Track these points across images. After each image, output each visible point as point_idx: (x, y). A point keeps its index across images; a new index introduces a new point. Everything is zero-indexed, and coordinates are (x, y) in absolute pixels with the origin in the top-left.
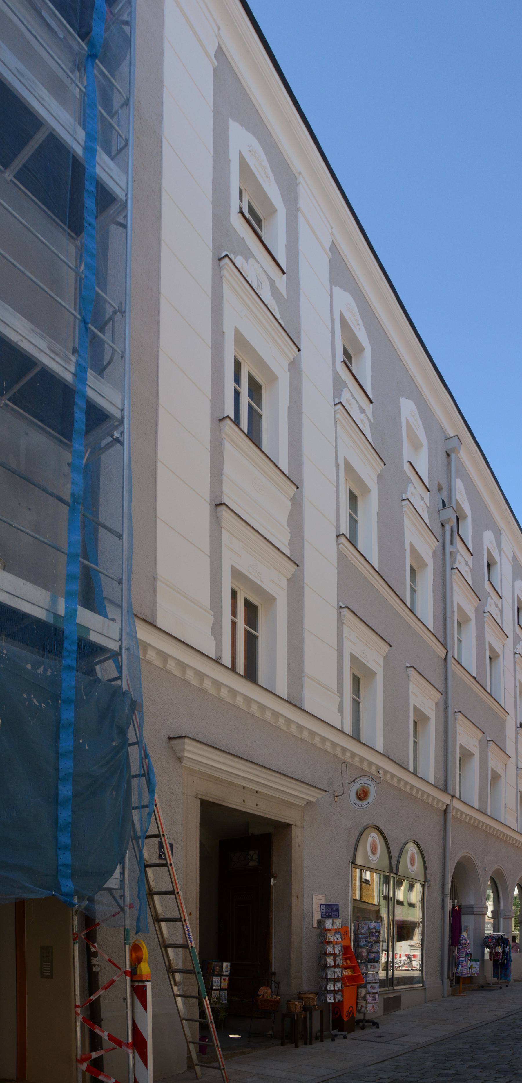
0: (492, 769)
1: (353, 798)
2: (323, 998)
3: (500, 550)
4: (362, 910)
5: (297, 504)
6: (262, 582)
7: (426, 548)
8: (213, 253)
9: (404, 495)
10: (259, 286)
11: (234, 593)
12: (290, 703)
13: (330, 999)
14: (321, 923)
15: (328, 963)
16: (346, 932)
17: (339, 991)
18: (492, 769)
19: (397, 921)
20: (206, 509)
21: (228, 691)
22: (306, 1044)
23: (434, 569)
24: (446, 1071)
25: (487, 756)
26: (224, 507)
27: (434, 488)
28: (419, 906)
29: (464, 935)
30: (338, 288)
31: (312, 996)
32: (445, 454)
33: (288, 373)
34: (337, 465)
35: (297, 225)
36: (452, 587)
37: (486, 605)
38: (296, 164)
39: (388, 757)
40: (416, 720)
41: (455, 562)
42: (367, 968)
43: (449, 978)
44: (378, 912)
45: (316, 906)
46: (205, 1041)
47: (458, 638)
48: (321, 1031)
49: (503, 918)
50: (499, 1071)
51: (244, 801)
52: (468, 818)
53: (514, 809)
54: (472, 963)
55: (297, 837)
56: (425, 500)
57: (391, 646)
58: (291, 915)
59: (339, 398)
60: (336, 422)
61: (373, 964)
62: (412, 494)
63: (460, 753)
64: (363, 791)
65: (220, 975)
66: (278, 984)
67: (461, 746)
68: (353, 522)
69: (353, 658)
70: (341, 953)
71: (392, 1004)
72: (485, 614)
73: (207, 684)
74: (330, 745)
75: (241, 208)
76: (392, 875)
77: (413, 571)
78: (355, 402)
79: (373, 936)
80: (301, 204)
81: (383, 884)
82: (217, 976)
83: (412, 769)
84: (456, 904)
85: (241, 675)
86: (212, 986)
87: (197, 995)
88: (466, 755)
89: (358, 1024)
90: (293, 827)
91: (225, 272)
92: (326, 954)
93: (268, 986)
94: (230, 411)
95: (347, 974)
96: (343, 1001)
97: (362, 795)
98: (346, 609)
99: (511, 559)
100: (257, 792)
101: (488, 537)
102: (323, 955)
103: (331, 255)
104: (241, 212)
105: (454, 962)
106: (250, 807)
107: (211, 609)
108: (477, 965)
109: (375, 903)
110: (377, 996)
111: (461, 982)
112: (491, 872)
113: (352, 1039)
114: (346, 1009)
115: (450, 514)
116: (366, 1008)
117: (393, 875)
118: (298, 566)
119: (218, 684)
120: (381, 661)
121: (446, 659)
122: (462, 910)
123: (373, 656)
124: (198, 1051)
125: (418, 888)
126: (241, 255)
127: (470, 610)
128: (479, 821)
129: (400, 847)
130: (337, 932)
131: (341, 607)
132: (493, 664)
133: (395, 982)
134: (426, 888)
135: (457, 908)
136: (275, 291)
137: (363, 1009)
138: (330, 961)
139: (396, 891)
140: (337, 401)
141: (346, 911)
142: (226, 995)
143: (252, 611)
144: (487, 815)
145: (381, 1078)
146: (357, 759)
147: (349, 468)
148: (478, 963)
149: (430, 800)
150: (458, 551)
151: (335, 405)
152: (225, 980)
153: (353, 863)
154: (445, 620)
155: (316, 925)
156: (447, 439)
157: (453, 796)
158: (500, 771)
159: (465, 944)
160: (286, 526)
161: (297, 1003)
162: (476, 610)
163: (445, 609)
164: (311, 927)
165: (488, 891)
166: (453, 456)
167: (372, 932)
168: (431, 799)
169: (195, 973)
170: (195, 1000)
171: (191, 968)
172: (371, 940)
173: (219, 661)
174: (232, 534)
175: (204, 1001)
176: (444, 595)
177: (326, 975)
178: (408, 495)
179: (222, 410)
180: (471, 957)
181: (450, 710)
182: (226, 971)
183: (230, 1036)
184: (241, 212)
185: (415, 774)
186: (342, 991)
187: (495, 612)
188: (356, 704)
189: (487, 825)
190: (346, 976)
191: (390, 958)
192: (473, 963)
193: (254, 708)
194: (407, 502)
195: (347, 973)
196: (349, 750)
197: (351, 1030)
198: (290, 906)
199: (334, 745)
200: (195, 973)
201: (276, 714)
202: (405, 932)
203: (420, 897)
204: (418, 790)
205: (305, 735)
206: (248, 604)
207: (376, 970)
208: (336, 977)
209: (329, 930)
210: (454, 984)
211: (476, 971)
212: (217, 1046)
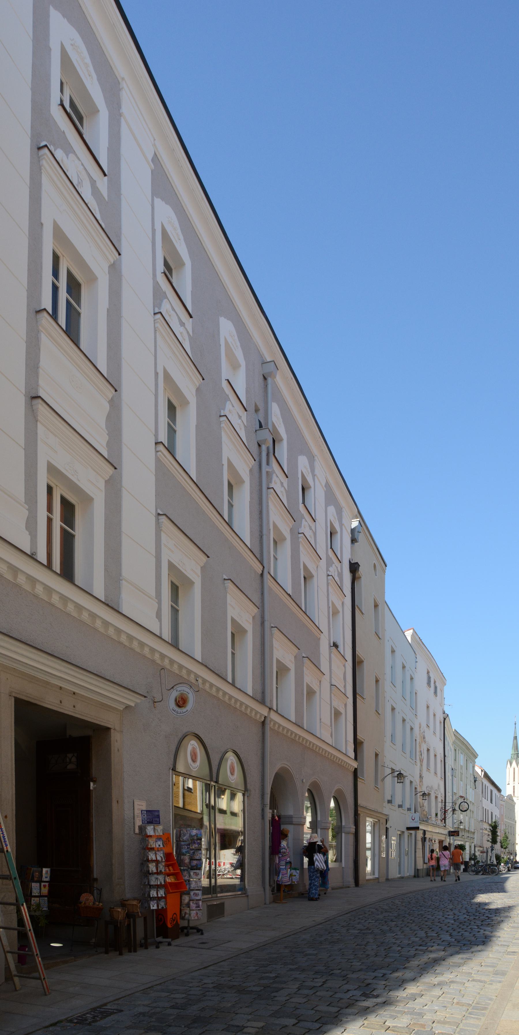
0: (308, 685)
1: (172, 705)
2: (146, 905)
3: (314, 476)
4: (184, 818)
5: (115, 405)
6: (79, 480)
7: (244, 466)
8: (32, 141)
9: (222, 411)
10: (79, 183)
11: (50, 490)
12: (107, 605)
13: (153, 906)
14: (142, 829)
15: (150, 870)
16: (168, 839)
17: (162, 897)
18: (308, 685)
19: (218, 829)
20: (21, 401)
21: (44, 588)
22: (130, 951)
23: (251, 486)
24: (267, 975)
25: (303, 672)
26: (40, 401)
27: (251, 409)
28: (241, 815)
29: (284, 843)
30: (159, 200)
31: (135, 903)
32: (262, 377)
33: (108, 276)
34: (157, 374)
35: (120, 130)
36: (268, 506)
37: (301, 526)
38: (120, 70)
39: (206, 666)
40: (233, 632)
41: (271, 482)
42: (190, 876)
43: (270, 886)
44: (202, 819)
45: (137, 812)
46: (25, 950)
47: (274, 556)
48: (146, 938)
49: (321, 829)
50: (316, 973)
51: (61, 702)
52: (285, 730)
53: (329, 724)
54: (292, 871)
55: (117, 741)
56: (242, 418)
57: (208, 557)
58: (112, 821)
59: (159, 308)
60: (155, 331)
61: (195, 871)
62: (230, 412)
63: (277, 667)
64: (182, 698)
65: (40, 881)
66: (100, 891)
67: (278, 661)
68: (172, 432)
69: (171, 566)
70: (164, 860)
71: (216, 911)
72: (300, 535)
73: (21, 579)
74: (148, 650)
75: (61, 101)
76: (213, 783)
77: (230, 486)
78: (175, 314)
79: (195, 843)
80: (124, 110)
81: (206, 792)
82: (36, 882)
83: (230, 679)
84: (275, 814)
85: (57, 574)
86: (31, 893)
87: (15, 902)
88: (282, 670)
89: (182, 931)
90: (112, 731)
91: (44, 162)
92: (148, 860)
93: (90, 893)
94: (47, 304)
95: (170, 881)
96: (166, 908)
97: (181, 702)
98: (164, 517)
99: (324, 485)
100: (74, 693)
101: (303, 461)
102: (145, 861)
103: (153, 166)
104: (62, 105)
105: (275, 871)
106: (67, 708)
107: (25, 503)
108: (296, 873)
109: (199, 811)
110: (200, 903)
111: (282, 889)
112: (308, 784)
113: (176, 946)
114: (170, 915)
115: (265, 435)
116: (190, 914)
117: (214, 784)
118: (115, 468)
119: (33, 581)
120: (199, 571)
121: (262, 575)
122: (282, 820)
123: (191, 566)
124: (17, 961)
125: (239, 796)
126: (62, 149)
127: (285, 530)
128: (296, 735)
129: (220, 756)
130: (159, 838)
131: (159, 514)
132: (307, 585)
133: (218, 890)
134: (246, 797)
135: (276, 818)
136: (95, 191)
137: (187, 916)
138: (152, 867)
139: (217, 799)
140: (157, 311)
141: (168, 818)
142: (46, 902)
143: (68, 509)
144: (303, 729)
145: (205, 984)
146: (176, 666)
147: (168, 377)
148: (298, 871)
149: (248, 712)
150: (274, 472)
151: (155, 314)
152: (45, 886)
153: (174, 769)
154: (261, 537)
155: (137, 831)
156: (264, 363)
157: (270, 709)
158: (315, 687)
159: (285, 853)
160: (104, 426)
161: (120, 910)
162: (291, 530)
163: (261, 526)
164: (132, 833)
165: (306, 802)
166: (269, 380)
167: (193, 839)
168: (249, 710)
169: (11, 879)
170: (12, 907)
171: (8, 873)
172: (193, 847)
173: (34, 556)
174: (48, 429)
175: (22, 908)
176: (261, 513)
177: (149, 882)
178: (226, 412)
179: (39, 302)
180: (291, 866)
181: (267, 625)
182: (46, 877)
183: (52, 944)
184: (62, 105)
185: (233, 684)
186: (165, 898)
187: (309, 534)
188: (175, 612)
189: (304, 738)
190: (169, 883)
191: (213, 867)
192: (293, 871)
193: (70, 608)
194: (225, 418)
195: (170, 880)
196: (215, 686)
197: (176, 937)
198: (111, 811)
199: (153, 650)
200: (11, 879)
201: (93, 616)
202: (227, 840)
203: (242, 808)
204: (236, 700)
205: (123, 639)
206: (65, 503)
207: (199, 877)
208: (159, 883)
209: (151, 836)
210: (276, 891)
211: (296, 879)
212: (37, 955)
